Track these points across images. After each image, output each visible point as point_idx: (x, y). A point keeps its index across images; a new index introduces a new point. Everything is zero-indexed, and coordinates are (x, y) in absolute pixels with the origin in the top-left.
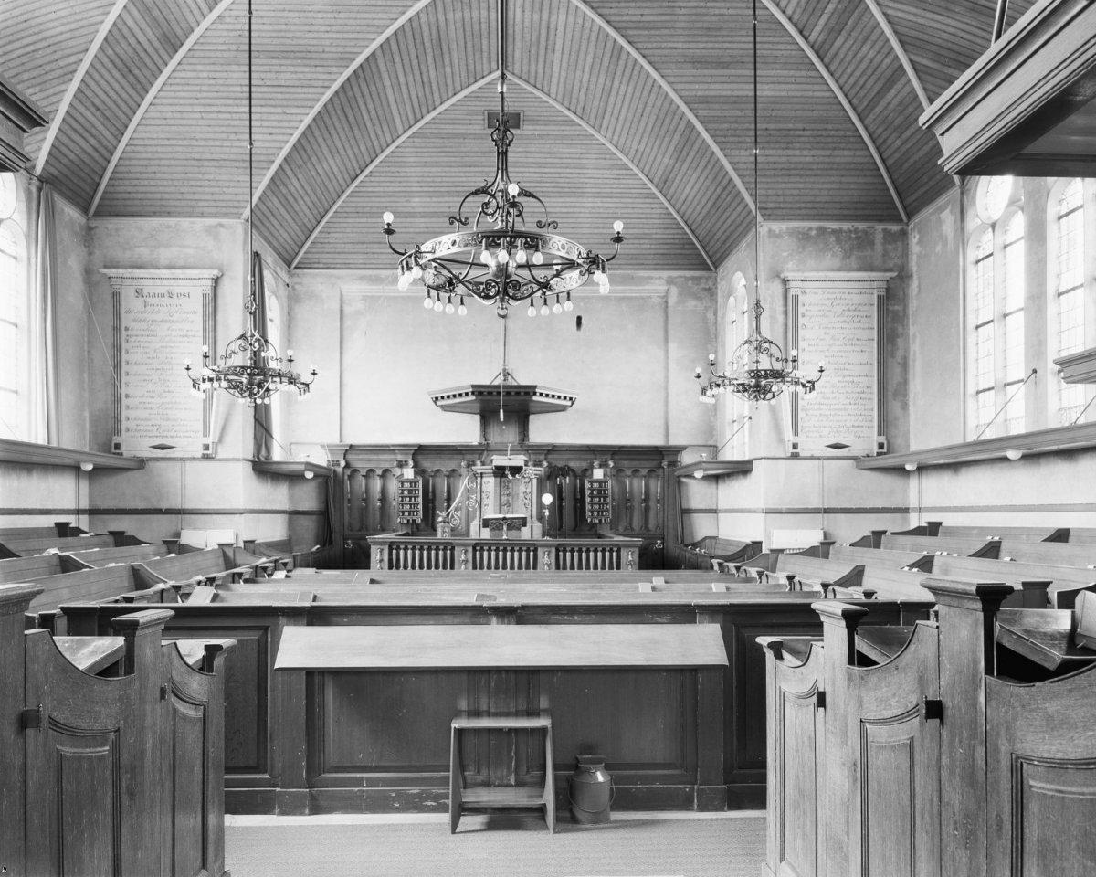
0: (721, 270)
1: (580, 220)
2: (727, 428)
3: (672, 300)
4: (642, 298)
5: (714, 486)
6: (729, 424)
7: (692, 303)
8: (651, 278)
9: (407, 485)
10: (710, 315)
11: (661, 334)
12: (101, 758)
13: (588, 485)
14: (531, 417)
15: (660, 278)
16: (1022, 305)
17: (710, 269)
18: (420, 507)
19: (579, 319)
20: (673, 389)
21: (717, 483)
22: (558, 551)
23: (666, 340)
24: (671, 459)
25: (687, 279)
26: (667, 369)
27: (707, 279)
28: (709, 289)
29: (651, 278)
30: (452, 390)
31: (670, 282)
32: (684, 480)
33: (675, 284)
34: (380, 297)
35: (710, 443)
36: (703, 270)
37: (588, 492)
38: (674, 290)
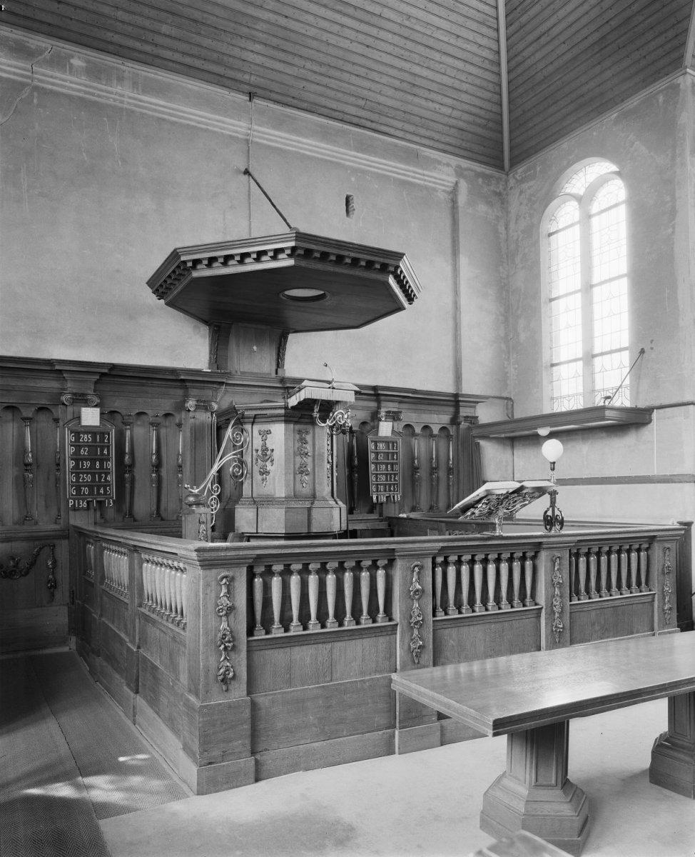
0: (520, 170)
1: (382, 34)
2: (544, 374)
3: (462, 198)
4: (426, 188)
5: (509, 452)
6: (546, 367)
7: (482, 208)
8: (439, 163)
9: (86, 438)
10: (501, 229)
11: (447, 243)
12: (229, 647)
13: (371, 446)
14: (291, 337)
15: (448, 165)
16: (627, 345)
17: (501, 168)
18: (112, 478)
19: (348, 200)
20: (465, 319)
21: (513, 447)
22: (251, 577)
23: (455, 253)
24: (216, 534)
25: (478, 175)
26: (456, 292)
27: (499, 179)
28: (500, 194)
29: (439, 163)
30: (220, 246)
31: (460, 172)
32: (482, 443)
33: (464, 177)
34: (23, 85)
35: (505, 395)
36: (495, 166)
37: (372, 456)
38: (463, 185)
